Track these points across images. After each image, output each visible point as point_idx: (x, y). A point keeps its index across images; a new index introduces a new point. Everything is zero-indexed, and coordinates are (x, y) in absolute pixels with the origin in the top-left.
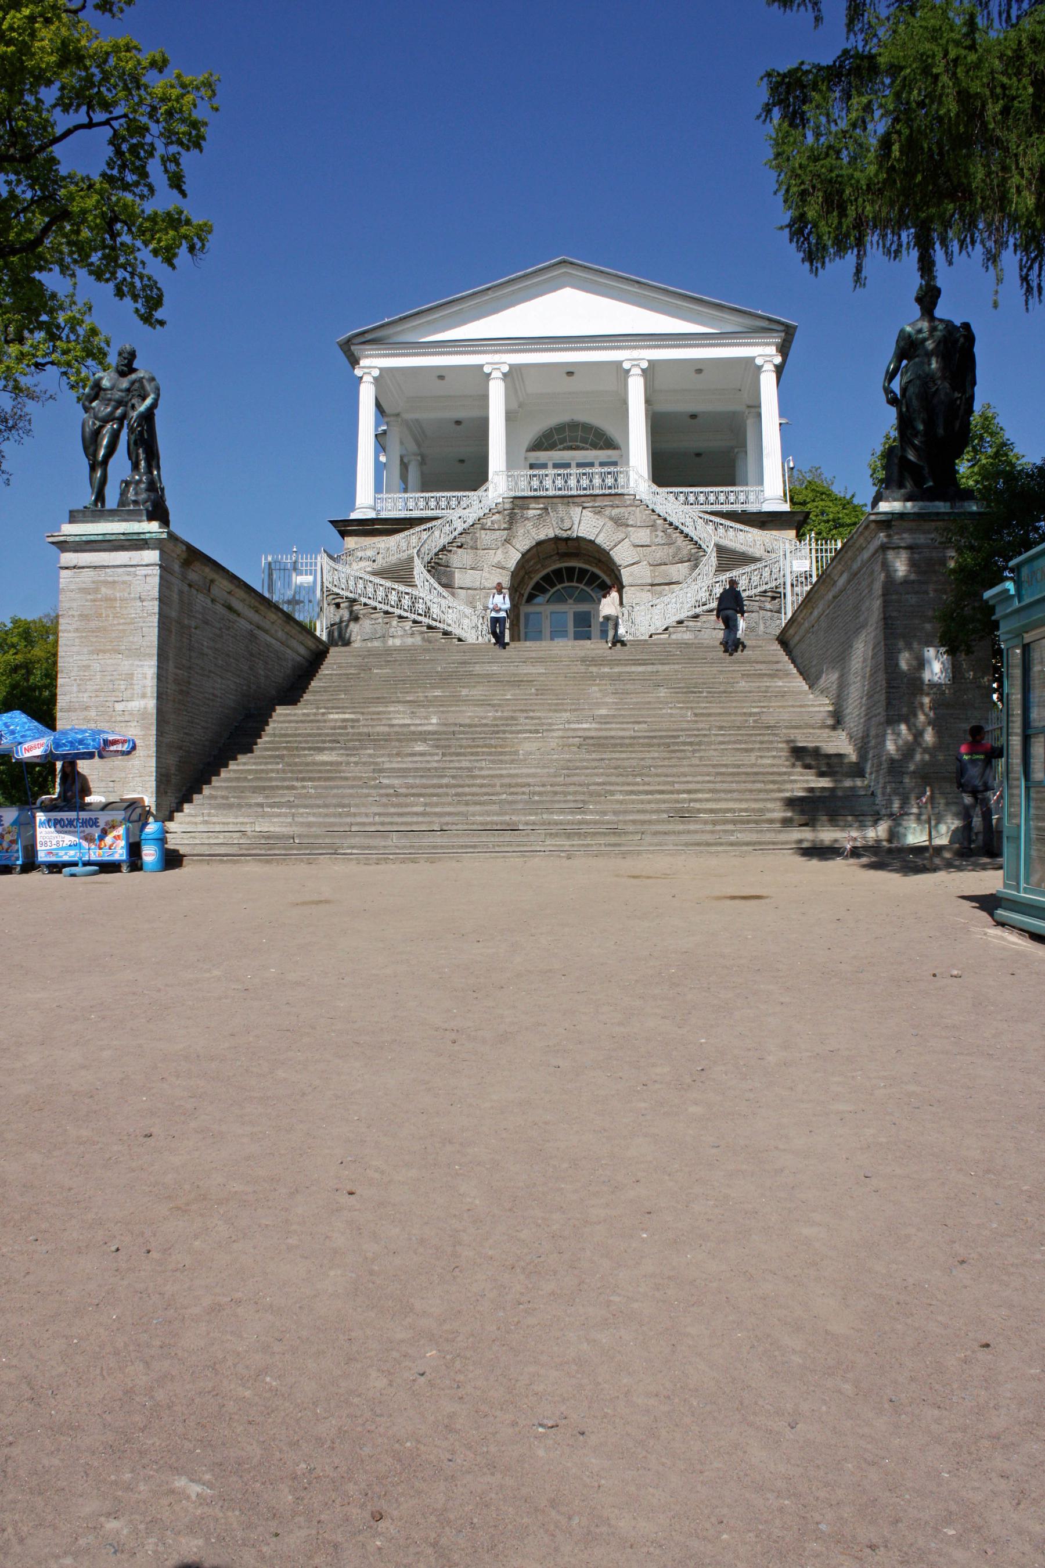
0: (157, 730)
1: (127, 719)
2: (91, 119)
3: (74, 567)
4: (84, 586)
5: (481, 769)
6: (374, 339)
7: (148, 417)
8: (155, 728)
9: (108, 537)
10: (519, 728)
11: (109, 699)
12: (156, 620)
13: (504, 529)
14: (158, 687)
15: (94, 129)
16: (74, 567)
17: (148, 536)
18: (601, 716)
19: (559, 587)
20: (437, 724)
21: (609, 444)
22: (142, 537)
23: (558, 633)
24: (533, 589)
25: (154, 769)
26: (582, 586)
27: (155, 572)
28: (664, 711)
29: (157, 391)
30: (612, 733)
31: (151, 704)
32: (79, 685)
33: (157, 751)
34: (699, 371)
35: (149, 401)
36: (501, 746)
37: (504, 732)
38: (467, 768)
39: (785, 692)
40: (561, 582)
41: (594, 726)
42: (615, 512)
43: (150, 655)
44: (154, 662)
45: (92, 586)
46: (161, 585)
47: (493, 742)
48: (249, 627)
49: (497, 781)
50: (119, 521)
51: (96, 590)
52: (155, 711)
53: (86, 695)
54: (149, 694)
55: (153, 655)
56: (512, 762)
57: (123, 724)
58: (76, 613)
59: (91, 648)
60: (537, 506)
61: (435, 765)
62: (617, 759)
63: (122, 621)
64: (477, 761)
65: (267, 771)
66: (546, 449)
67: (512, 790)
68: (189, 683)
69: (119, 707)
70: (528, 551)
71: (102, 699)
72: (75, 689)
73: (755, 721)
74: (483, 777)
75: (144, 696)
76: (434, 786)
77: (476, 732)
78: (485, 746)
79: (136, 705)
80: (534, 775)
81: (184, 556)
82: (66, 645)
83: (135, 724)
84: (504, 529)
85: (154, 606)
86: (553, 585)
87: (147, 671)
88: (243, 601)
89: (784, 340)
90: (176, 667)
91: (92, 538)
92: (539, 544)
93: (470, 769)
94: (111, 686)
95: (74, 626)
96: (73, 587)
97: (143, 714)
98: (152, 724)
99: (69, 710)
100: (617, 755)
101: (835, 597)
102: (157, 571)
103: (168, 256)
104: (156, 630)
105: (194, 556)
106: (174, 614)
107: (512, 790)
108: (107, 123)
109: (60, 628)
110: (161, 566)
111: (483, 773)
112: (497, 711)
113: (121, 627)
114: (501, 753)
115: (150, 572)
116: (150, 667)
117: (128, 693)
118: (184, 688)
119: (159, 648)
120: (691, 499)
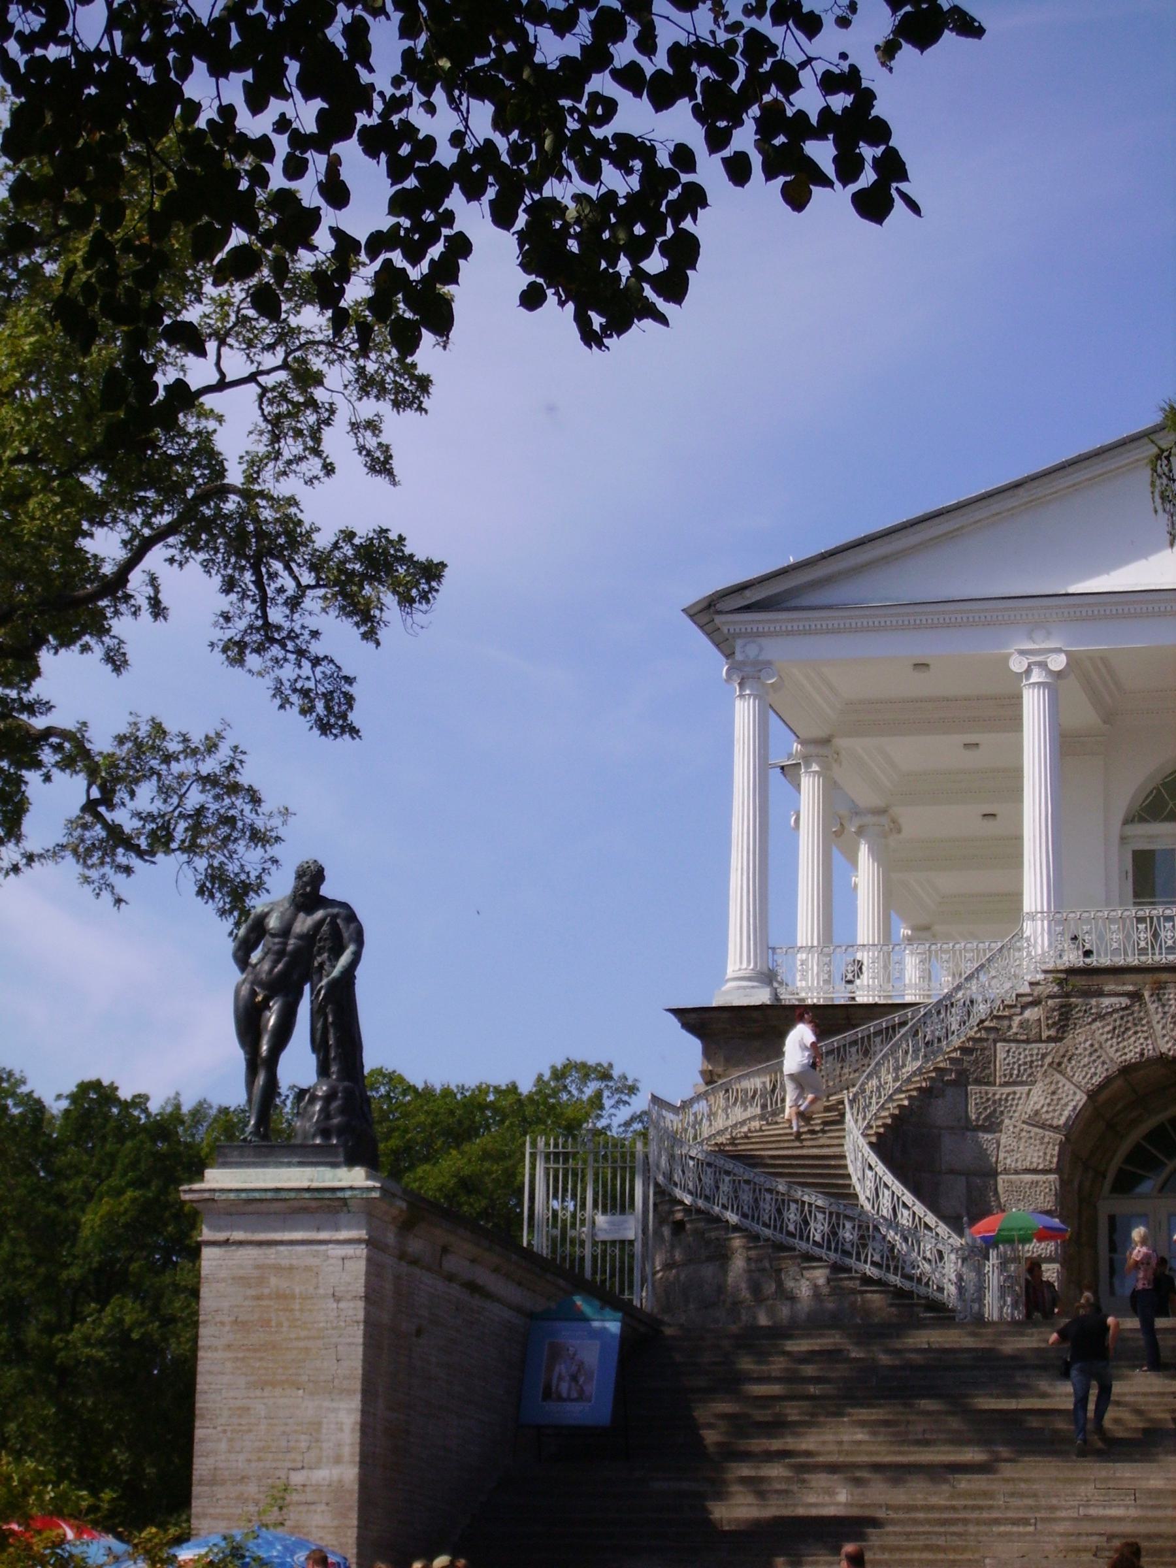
0: (360, 1518)
2: (223, 375)
4: (241, 1273)
7: (349, 975)
9: (284, 1195)
10: (995, 1514)
12: (360, 1333)
13: (1050, 1039)
14: (362, 1444)
15: (228, 392)
17: (348, 1194)
18: (1150, 1493)
20: (846, 1505)
22: (340, 1195)
27: (358, 1252)
31: (350, 1473)
32: (231, 1440)
35: (344, 959)
37: (965, 1521)
41: (1133, 1512)
44: (356, 1402)
46: (368, 1273)
47: (941, 1542)
50: (301, 1164)
51: (261, 1281)
52: (356, 1487)
53: (241, 1457)
55: (354, 1391)
57: (301, 1508)
58: (226, 1319)
60: (1120, 989)
63: (303, 1333)
70: (1101, 1087)
72: (223, 1446)
75: (338, 1460)
77: (915, 1522)
78: (927, 1548)
79: (322, 1475)
82: (210, 1373)
83: (323, 1507)
84: (1050, 1039)
87: (343, 1419)
88: (496, 1270)
91: (257, 1195)
92: (1127, 1070)
96: (223, 1274)
97: (337, 1488)
102: (362, 1251)
103: (365, 618)
104: (360, 1349)
108: (252, 378)
109: (201, 1343)
110: (369, 1243)
113: (301, 1344)
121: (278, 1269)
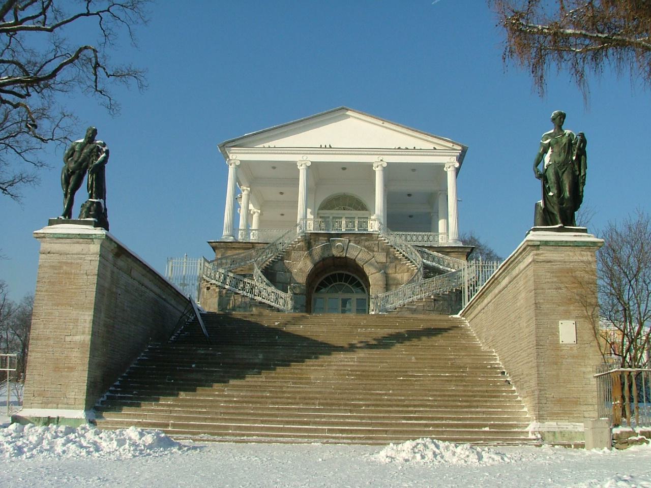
1: (72, 346)
3: (49, 253)
4: (53, 264)
5: (288, 387)
6: (239, 142)
8: (89, 353)
11: (62, 334)
12: (95, 287)
16: (49, 253)
19: (334, 284)
21: (363, 207)
23: (333, 310)
24: (319, 285)
25: (86, 378)
26: (347, 284)
28: (397, 356)
29: (107, 152)
30: (367, 368)
31: (88, 338)
33: (89, 368)
34: (414, 170)
36: (301, 374)
38: (279, 386)
39: (467, 347)
40: (336, 281)
42: (367, 243)
43: (90, 308)
44: (92, 313)
45: (59, 265)
48: (155, 297)
49: (298, 396)
51: (61, 267)
54: (87, 332)
56: (307, 384)
57: (70, 350)
59: (53, 302)
61: (260, 384)
62: (370, 384)
63: (74, 287)
64: (285, 382)
65: (227, 428)
66: (329, 209)
67: (306, 401)
68: (114, 327)
69: (68, 339)
71: (58, 333)
72: (42, 326)
73: (452, 364)
74: (289, 392)
75: (83, 333)
76: (258, 397)
79: (78, 338)
80: (320, 393)
81: (116, 250)
82: (39, 300)
85: (94, 279)
86: (331, 283)
87: (86, 318)
89: (461, 155)
90: (106, 317)
93: (281, 387)
94: (64, 326)
95: (45, 289)
97: (82, 344)
98: (87, 351)
99: (37, 339)
100: (370, 382)
101: (500, 292)
104: (95, 293)
105: (121, 251)
106: (107, 285)
107: (306, 401)
111: (289, 390)
112: (298, 353)
113: (73, 291)
114: (300, 378)
115: (93, 258)
116: (89, 315)
117: (74, 331)
118: (110, 330)
119: (95, 304)
120: (409, 238)
121: (67, 263)
